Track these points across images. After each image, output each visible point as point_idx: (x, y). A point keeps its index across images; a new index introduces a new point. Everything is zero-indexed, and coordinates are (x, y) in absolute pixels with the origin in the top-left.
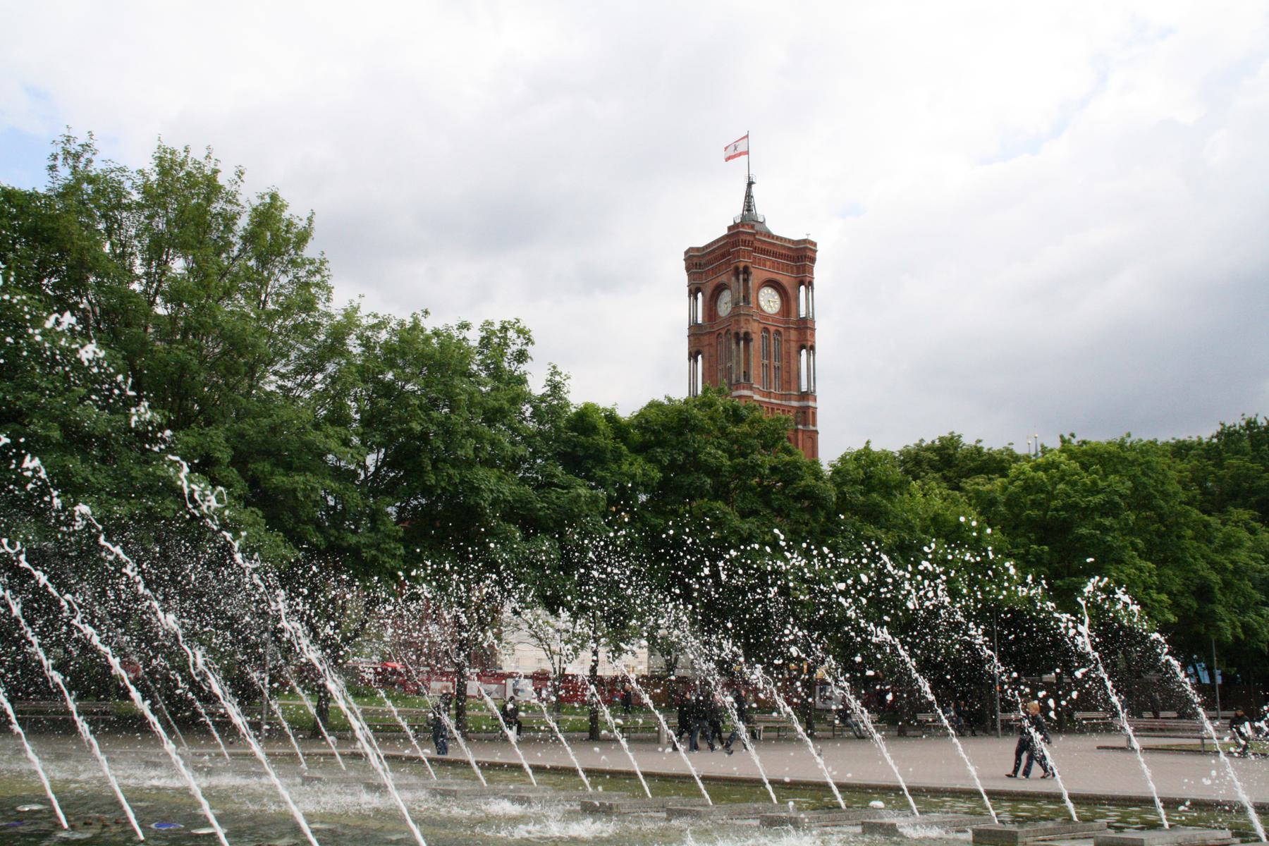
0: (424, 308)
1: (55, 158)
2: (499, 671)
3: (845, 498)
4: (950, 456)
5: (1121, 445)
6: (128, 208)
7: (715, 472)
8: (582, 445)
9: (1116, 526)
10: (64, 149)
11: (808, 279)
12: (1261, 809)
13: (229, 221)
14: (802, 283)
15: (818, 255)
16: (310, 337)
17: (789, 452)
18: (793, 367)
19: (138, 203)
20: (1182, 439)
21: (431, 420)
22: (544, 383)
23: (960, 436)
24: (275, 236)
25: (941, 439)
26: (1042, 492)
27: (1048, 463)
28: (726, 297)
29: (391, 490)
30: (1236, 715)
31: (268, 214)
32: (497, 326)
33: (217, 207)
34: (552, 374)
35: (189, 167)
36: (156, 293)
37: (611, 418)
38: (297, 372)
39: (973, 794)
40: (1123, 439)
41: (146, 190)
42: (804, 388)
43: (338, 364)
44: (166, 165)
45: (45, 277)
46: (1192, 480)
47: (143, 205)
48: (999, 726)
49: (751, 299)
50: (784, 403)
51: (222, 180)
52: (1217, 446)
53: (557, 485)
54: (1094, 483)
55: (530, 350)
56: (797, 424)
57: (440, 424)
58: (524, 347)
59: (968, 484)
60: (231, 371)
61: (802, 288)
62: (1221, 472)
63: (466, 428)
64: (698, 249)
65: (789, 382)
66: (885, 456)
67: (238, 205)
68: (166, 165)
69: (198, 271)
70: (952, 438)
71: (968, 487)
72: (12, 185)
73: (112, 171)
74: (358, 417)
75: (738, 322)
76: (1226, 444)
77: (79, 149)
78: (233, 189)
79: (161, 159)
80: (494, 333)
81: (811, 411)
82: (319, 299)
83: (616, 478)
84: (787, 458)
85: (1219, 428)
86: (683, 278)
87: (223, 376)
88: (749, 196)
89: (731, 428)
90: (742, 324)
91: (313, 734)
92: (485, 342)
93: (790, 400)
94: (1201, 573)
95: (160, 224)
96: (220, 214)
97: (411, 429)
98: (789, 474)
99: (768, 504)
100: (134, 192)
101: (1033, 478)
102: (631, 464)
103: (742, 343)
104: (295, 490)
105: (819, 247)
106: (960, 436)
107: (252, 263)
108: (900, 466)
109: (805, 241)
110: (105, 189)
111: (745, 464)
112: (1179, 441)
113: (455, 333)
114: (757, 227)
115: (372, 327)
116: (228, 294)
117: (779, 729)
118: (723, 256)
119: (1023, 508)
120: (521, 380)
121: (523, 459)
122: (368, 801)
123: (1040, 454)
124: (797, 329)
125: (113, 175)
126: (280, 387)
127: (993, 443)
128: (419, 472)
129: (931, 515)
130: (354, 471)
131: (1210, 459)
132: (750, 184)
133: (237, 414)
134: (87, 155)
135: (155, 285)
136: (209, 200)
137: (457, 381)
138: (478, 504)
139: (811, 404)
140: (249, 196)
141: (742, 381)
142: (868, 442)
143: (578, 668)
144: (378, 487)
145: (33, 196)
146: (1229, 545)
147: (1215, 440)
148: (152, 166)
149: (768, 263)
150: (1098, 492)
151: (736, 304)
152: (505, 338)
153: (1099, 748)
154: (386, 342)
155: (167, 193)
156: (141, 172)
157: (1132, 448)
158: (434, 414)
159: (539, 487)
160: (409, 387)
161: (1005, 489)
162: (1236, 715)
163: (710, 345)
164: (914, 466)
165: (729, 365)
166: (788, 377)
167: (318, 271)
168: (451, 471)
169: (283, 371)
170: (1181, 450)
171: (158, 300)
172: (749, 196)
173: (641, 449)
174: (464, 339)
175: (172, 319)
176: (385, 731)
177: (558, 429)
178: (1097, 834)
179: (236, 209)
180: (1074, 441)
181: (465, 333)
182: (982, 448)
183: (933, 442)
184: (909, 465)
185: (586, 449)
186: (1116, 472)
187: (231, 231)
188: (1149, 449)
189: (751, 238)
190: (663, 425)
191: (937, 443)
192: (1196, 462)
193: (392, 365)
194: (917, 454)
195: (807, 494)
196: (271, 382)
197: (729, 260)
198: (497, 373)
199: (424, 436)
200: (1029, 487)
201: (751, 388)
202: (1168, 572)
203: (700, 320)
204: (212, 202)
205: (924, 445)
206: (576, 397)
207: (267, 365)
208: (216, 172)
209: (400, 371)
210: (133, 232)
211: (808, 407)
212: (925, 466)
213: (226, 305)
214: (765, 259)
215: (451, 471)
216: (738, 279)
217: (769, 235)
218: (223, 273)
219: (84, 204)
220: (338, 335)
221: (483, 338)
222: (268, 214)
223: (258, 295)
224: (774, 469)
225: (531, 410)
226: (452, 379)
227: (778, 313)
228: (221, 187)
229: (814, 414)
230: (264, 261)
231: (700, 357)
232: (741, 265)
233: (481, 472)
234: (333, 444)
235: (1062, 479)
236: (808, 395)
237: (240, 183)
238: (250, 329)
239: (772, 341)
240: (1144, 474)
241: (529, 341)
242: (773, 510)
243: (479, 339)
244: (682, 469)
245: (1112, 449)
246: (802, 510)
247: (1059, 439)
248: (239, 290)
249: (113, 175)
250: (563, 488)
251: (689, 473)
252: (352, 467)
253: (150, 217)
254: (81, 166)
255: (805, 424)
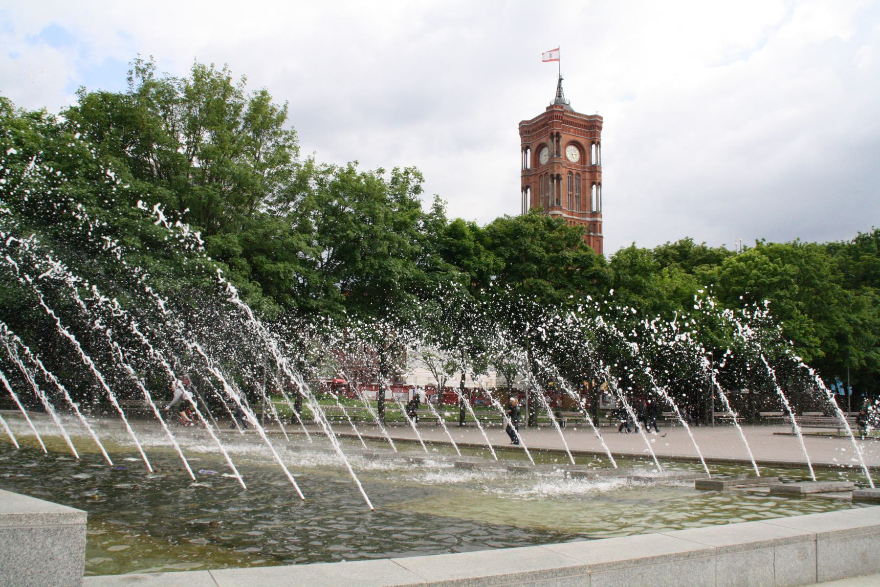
0: (355, 160)
1: (131, 73)
2: (404, 385)
3: (619, 278)
4: (686, 252)
5: (794, 245)
6: (176, 102)
7: (538, 261)
8: (455, 245)
9: (788, 295)
10: (136, 67)
11: (597, 140)
12: (872, 469)
13: (237, 108)
14: (593, 143)
15: (604, 125)
16: (286, 179)
17: (586, 250)
18: (588, 195)
19: (183, 99)
20: (832, 242)
21: (361, 229)
22: (431, 206)
23: (692, 239)
24: (265, 117)
25: (680, 241)
26: (743, 275)
27: (747, 257)
28: (545, 152)
29: (337, 273)
30: (860, 414)
31: (260, 105)
32: (402, 171)
33: (230, 100)
34: (436, 201)
35: (214, 76)
36: (193, 155)
37: (473, 228)
38: (280, 201)
39: (697, 461)
40: (795, 242)
41: (187, 91)
42: (594, 209)
43: (303, 196)
44: (199, 75)
45: (127, 146)
46: (839, 268)
47: (186, 101)
48: (714, 420)
49: (561, 153)
50: (581, 218)
51: (232, 84)
52: (855, 247)
53: (439, 270)
54: (775, 269)
55: (422, 185)
56: (589, 232)
57: (367, 232)
58: (419, 184)
59: (698, 270)
60: (239, 201)
61: (594, 146)
62: (858, 263)
63: (384, 234)
64: (527, 122)
65: (585, 206)
66: (644, 252)
67: (243, 99)
68: (199, 75)
69: (218, 139)
70: (687, 241)
71: (697, 272)
72: (107, 90)
73: (168, 79)
74: (316, 228)
75: (553, 167)
76: (861, 245)
77: (145, 67)
78: (239, 89)
79: (195, 71)
80: (400, 175)
81: (598, 224)
82: (291, 155)
83: (477, 266)
84: (584, 253)
85: (857, 235)
86: (517, 140)
87: (234, 205)
88: (559, 88)
89: (547, 234)
90: (555, 169)
91: (294, 421)
92: (395, 181)
93: (585, 217)
94: (841, 326)
95: (195, 112)
96: (231, 104)
97: (348, 235)
98: (584, 263)
99: (571, 281)
100: (180, 92)
101: (737, 267)
102: (487, 257)
103: (555, 181)
104: (278, 272)
105: (604, 120)
106: (692, 239)
107: (251, 134)
108: (654, 259)
109: (595, 116)
110: (163, 91)
111: (558, 257)
112: (830, 244)
113: (376, 175)
114: (565, 107)
115: (324, 173)
116: (236, 153)
117: (576, 421)
118: (543, 126)
119: (730, 285)
120: (417, 205)
121: (418, 254)
122: (325, 459)
123: (743, 251)
124: (590, 172)
125: (169, 82)
126: (269, 211)
127: (713, 244)
128: (354, 261)
129: (674, 288)
130: (315, 262)
131: (850, 255)
132: (560, 80)
133: (243, 227)
134: (150, 70)
135: (192, 149)
136: (224, 96)
137: (377, 206)
138: (391, 281)
139: (599, 219)
140: (249, 94)
141: (555, 204)
142: (634, 243)
143: (453, 382)
144: (328, 271)
145: (118, 97)
146: (857, 308)
147: (854, 243)
148: (190, 76)
149: (572, 130)
150: (777, 275)
151: (551, 157)
152: (407, 178)
153: (775, 434)
154: (332, 182)
155: (199, 92)
156: (184, 80)
157: (801, 247)
158: (363, 226)
159: (428, 271)
160: (347, 209)
161: (720, 273)
162: (860, 414)
163: (535, 182)
164: (663, 258)
165: (547, 195)
166: (583, 202)
167: (291, 138)
168: (373, 261)
169: (270, 200)
170: (832, 249)
171: (195, 159)
172: (559, 88)
173: (492, 247)
174: (381, 179)
175: (203, 171)
176: (336, 420)
177: (439, 235)
178: (772, 484)
179: (241, 101)
180: (765, 243)
181: (382, 176)
182: (706, 247)
183: (676, 243)
184: (660, 258)
185: (457, 247)
186: (790, 262)
187: (238, 115)
188: (811, 248)
189: (561, 115)
190: (505, 233)
191: (678, 244)
192: (841, 257)
193: (337, 196)
194: (665, 251)
195: (596, 275)
196: (263, 207)
197: (547, 128)
198: (402, 201)
199: (357, 240)
200: (736, 272)
201: (561, 209)
202: (821, 325)
203: (529, 167)
204: (227, 98)
205: (670, 245)
206: (451, 216)
207: (261, 196)
208: (229, 79)
209: (341, 199)
210: (179, 117)
211: (597, 221)
212: (670, 258)
213: (236, 161)
214: (570, 128)
215: (373, 261)
216: (553, 141)
217: (573, 112)
218: (233, 140)
219: (150, 100)
220: (303, 179)
221: (393, 178)
222: (260, 105)
223: (254, 154)
224: (575, 260)
225: (423, 223)
226: (374, 204)
227: (578, 162)
228: (233, 88)
229: (600, 226)
230: (257, 132)
231: (529, 190)
232: (555, 132)
233: (393, 261)
234: (303, 244)
235: (756, 267)
236: (595, 214)
237: (244, 85)
238: (250, 174)
239: (574, 180)
240: (807, 263)
241: (421, 180)
242: (575, 285)
243: (391, 179)
244: (517, 260)
245: (788, 248)
246: (592, 285)
247: (755, 242)
248: (242, 151)
249: (169, 82)
250: (443, 271)
251: (522, 263)
252: (314, 259)
253: (190, 108)
254: (146, 77)
255: (595, 232)
